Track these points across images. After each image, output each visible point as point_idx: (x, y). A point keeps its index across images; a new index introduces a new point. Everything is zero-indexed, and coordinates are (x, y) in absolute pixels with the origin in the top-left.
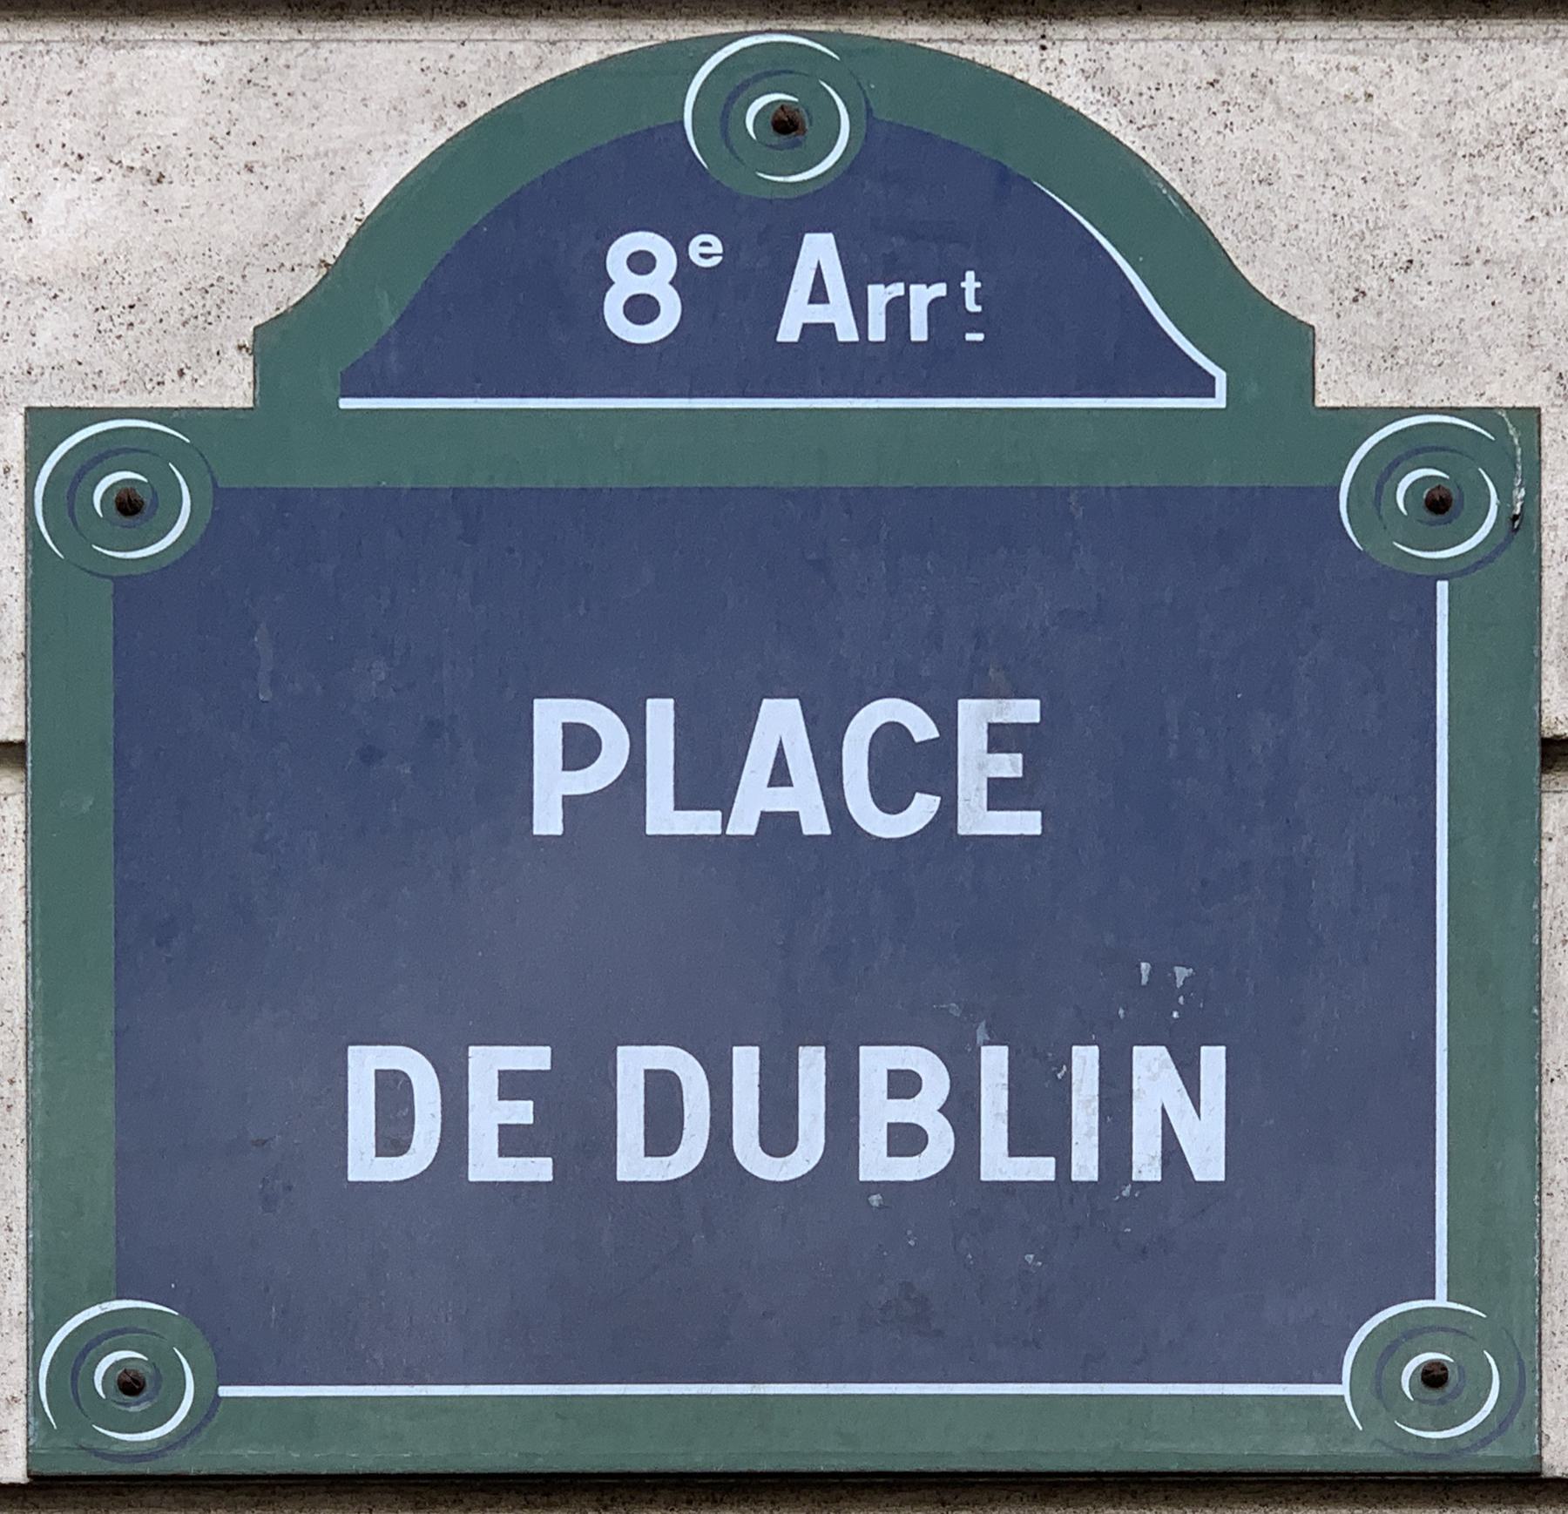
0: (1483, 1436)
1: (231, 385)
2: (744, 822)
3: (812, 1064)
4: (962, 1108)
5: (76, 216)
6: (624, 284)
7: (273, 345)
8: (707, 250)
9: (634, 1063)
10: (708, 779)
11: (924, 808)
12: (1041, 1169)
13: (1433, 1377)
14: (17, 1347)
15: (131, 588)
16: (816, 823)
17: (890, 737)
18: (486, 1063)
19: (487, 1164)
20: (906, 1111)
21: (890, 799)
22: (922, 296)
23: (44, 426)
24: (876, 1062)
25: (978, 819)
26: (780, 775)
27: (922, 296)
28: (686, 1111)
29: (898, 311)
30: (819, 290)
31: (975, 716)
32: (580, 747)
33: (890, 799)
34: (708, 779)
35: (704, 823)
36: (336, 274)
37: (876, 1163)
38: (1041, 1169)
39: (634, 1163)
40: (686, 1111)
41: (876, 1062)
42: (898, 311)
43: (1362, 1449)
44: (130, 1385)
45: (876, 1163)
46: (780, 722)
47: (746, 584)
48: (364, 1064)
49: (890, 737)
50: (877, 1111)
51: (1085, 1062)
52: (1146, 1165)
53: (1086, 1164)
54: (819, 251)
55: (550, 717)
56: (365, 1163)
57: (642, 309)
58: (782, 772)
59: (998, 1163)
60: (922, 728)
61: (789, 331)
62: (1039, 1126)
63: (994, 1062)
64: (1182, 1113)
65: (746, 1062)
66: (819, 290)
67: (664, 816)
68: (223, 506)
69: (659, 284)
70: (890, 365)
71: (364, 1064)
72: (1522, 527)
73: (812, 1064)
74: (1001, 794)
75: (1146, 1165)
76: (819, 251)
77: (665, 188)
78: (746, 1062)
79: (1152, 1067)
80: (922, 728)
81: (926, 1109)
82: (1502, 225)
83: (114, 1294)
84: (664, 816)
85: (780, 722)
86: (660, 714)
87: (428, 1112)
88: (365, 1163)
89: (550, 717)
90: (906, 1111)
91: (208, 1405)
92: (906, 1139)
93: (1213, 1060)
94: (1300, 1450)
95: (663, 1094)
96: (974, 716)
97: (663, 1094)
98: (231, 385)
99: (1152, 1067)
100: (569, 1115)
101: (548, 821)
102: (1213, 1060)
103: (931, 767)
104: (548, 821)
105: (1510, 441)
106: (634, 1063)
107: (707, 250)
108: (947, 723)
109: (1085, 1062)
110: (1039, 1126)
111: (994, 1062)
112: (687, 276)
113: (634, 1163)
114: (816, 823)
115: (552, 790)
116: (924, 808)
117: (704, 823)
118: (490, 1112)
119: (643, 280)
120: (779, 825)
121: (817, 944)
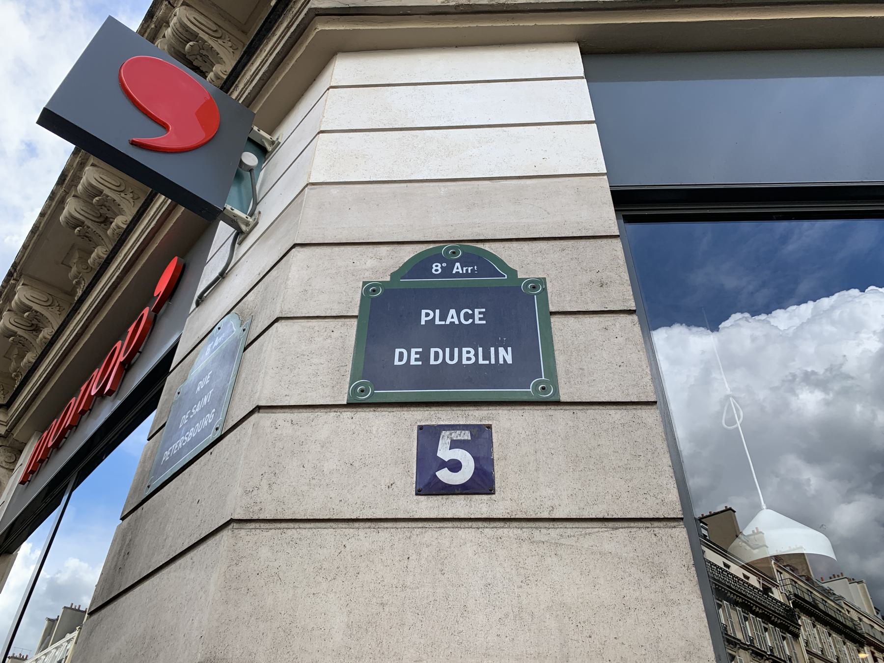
0: (551, 396)
1: (388, 279)
2: (448, 322)
3: (456, 350)
4: (476, 355)
5: (370, 263)
6: (434, 268)
7: (392, 275)
8: (444, 265)
9: (433, 350)
10: (443, 317)
11: (470, 321)
12: (487, 362)
13: (543, 388)
14: (347, 386)
15: (373, 299)
16: (457, 322)
17: (466, 314)
18: (413, 351)
19: (413, 362)
20: (468, 355)
21: (466, 320)
22: (470, 269)
23: (364, 283)
24: (465, 350)
25: (477, 322)
26: (452, 317)
27: (470, 269)
28: (438, 356)
29: (467, 270)
30: (457, 268)
31: (477, 311)
32: (427, 315)
33: (466, 320)
34: (443, 317)
35: (443, 323)
36: (401, 268)
37: (465, 362)
38: (487, 362)
39: (432, 362)
40: (438, 356)
41: (465, 350)
42: (467, 270)
43: (534, 398)
44: (362, 391)
45: (465, 362)
46: (452, 312)
47: (445, 298)
48: (397, 351)
49: (466, 314)
50: (465, 355)
51: (492, 349)
52: (501, 361)
53: (493, 361)
54: (458, 264)
55: (424, 312)
56: (397, 362)
57: (437, 270)
58: (452, 317)
59: (481, 361)
60: (470, 312)
61: (454, 272)
62: (486, 356)
63: (480, 349)
64: (506, 355)
65: (448, 350)
66: (457, 268)
67: (437, 322)
68: (385, 291)
69: (439, 268)
70: (467, 275)
71: (397, 351)
72: (545, 290)
73: (456, 350)
74: (480, 319)
75: (501, 361)
76: (458, 264)
77: (439, 258)
78: (448, 350)
79: (501, 350)
80: (470, 312)
81: (471, 355)
82: (539, 260)
83: (478, 466)
84: (437, 322)
85: (452, 312)
86: (437, 311)
87: (406, 357)
88: (397, 362)
89: (424, 312)
90: (468, 355)
91: (373, 393)
92: (469, 359)
93: (509, 349)
94: (525, 398)
95: (437, 354)
96: (477, 311)
97: (437, 354)
98: (388, 279)
99: (501, 350)
100: (424, 357)
101: (423, 323)
102: (509, 349)
103: (472, 316)
104: (423, 323)
105: (543, 281)
106: (433, 350)
107: (444, 265)
108: (474, 312)
109: (492, 349)
110: (486, 356)
111: (480, 349)
112: (442, 267)
113: (432, 362)
114: (457, 322)
115: (423, 320)
116: (470, 321)
117: (443, 323)
118: (413, 356)
119: (437, 268)
120: (452, 323)
121: (454, 337)
